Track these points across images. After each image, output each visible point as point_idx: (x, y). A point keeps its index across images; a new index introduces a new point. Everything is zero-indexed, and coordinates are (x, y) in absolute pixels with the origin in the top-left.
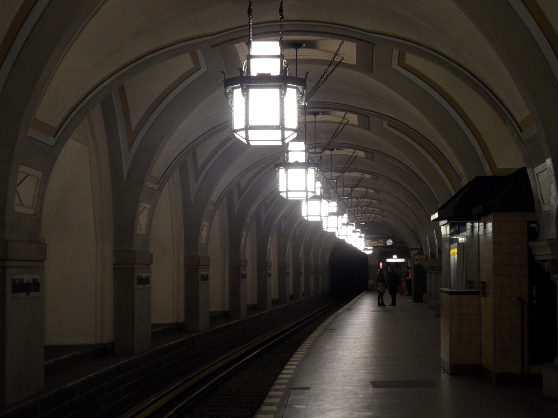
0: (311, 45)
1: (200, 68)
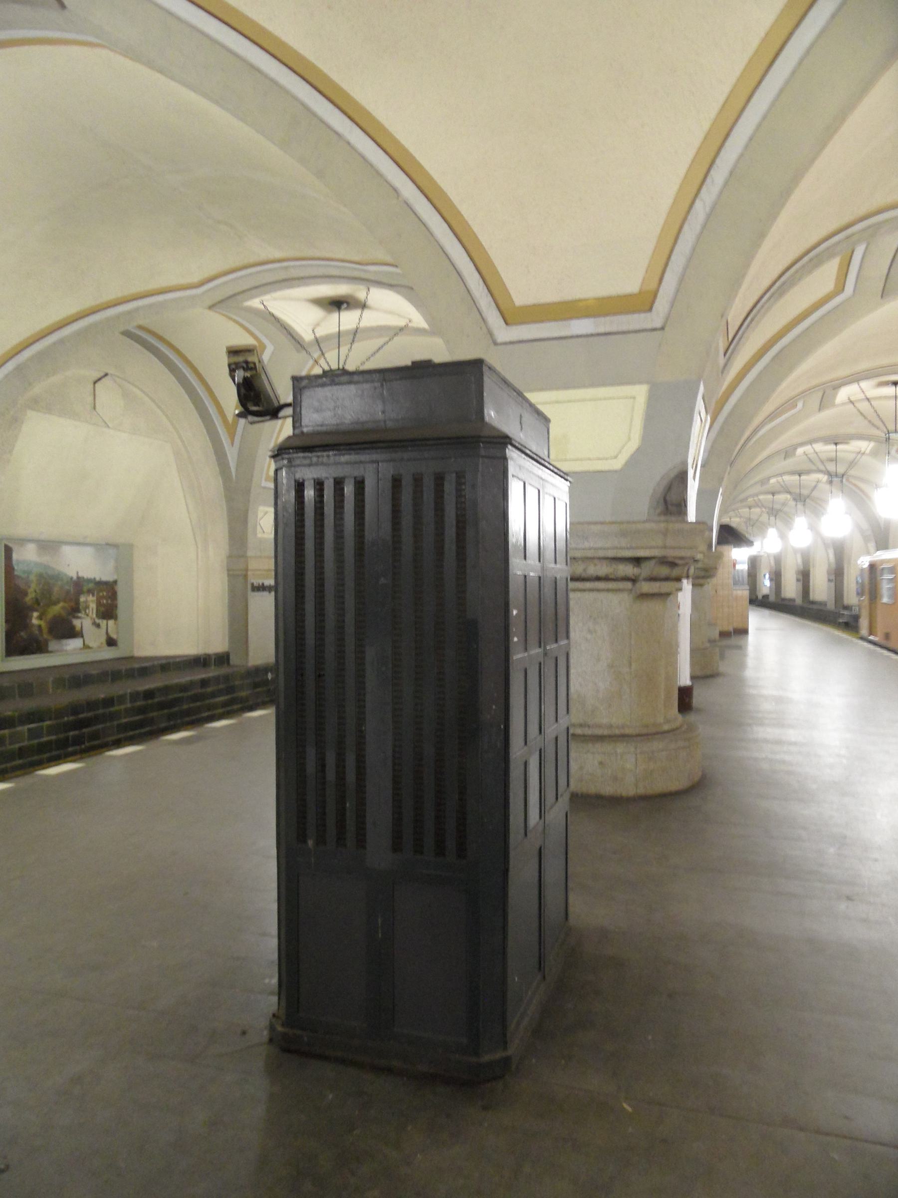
1: (507, 323)
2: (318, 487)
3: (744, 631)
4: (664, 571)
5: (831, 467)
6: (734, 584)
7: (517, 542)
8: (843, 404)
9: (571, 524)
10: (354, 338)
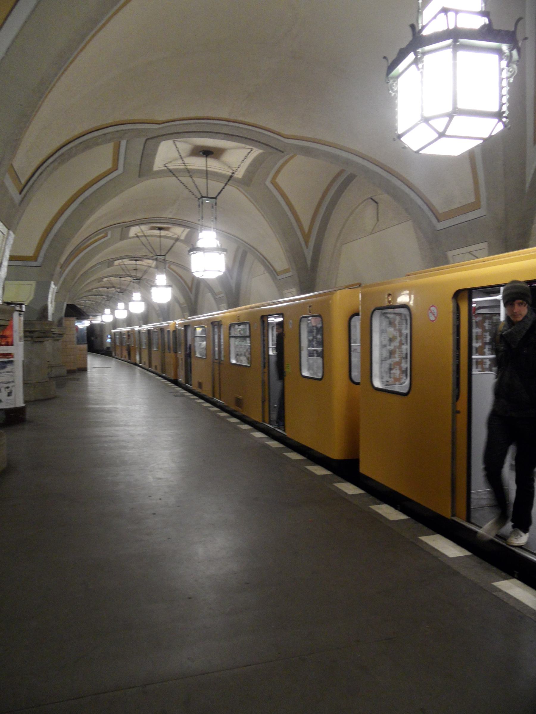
0: (167, 229)
2: (520, 305)
3: (84, 370)
4: (42, 335)
5: (134, 274)
6: (78, 341)
7: (490, 328)
8: (133, 237)
9: (219, 310)
10: (228, 182)
